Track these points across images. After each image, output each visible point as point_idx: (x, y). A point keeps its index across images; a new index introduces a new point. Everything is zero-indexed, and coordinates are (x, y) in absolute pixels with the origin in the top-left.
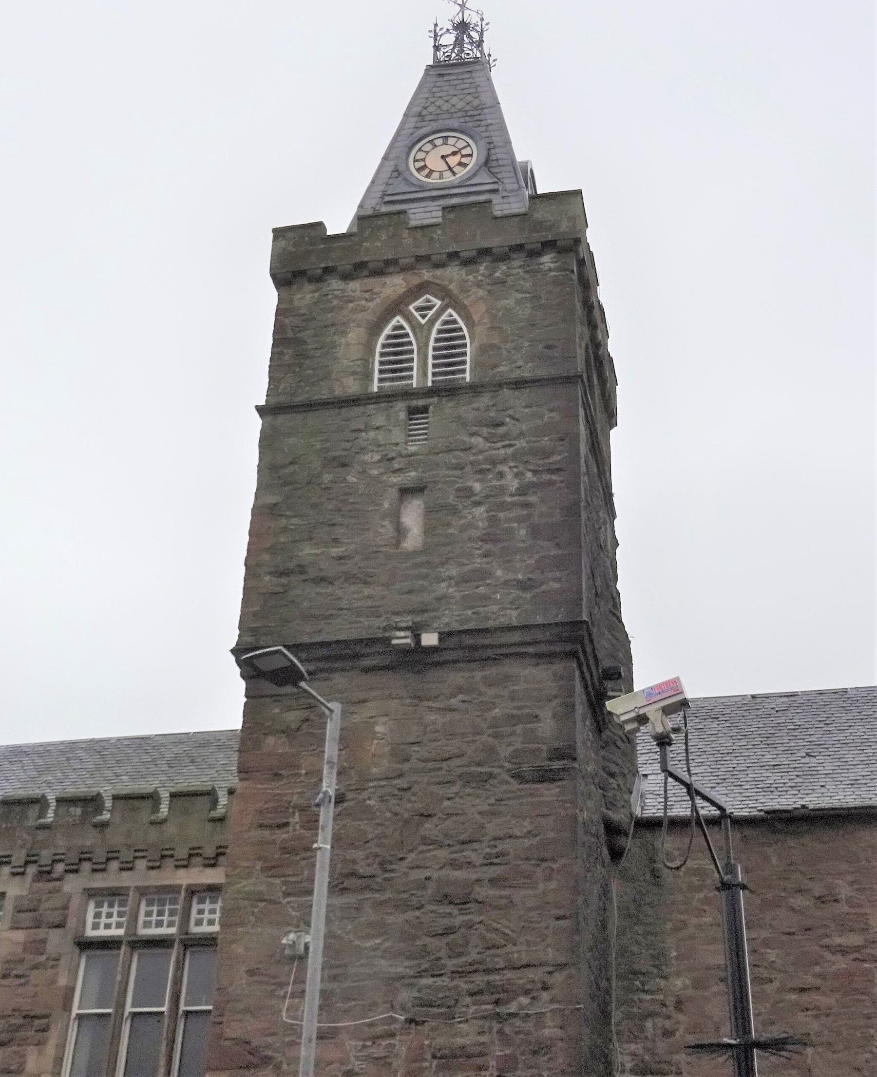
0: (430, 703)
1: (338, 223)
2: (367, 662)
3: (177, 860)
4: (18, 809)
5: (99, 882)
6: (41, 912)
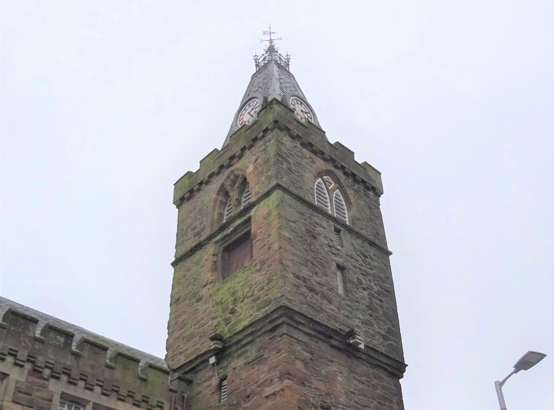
0: (354, 375)
1: (220, 149)
2: (333, 342)
3: (135, 400)
4: (22, 321)
5: (71, 391)
6: (33, 397)
